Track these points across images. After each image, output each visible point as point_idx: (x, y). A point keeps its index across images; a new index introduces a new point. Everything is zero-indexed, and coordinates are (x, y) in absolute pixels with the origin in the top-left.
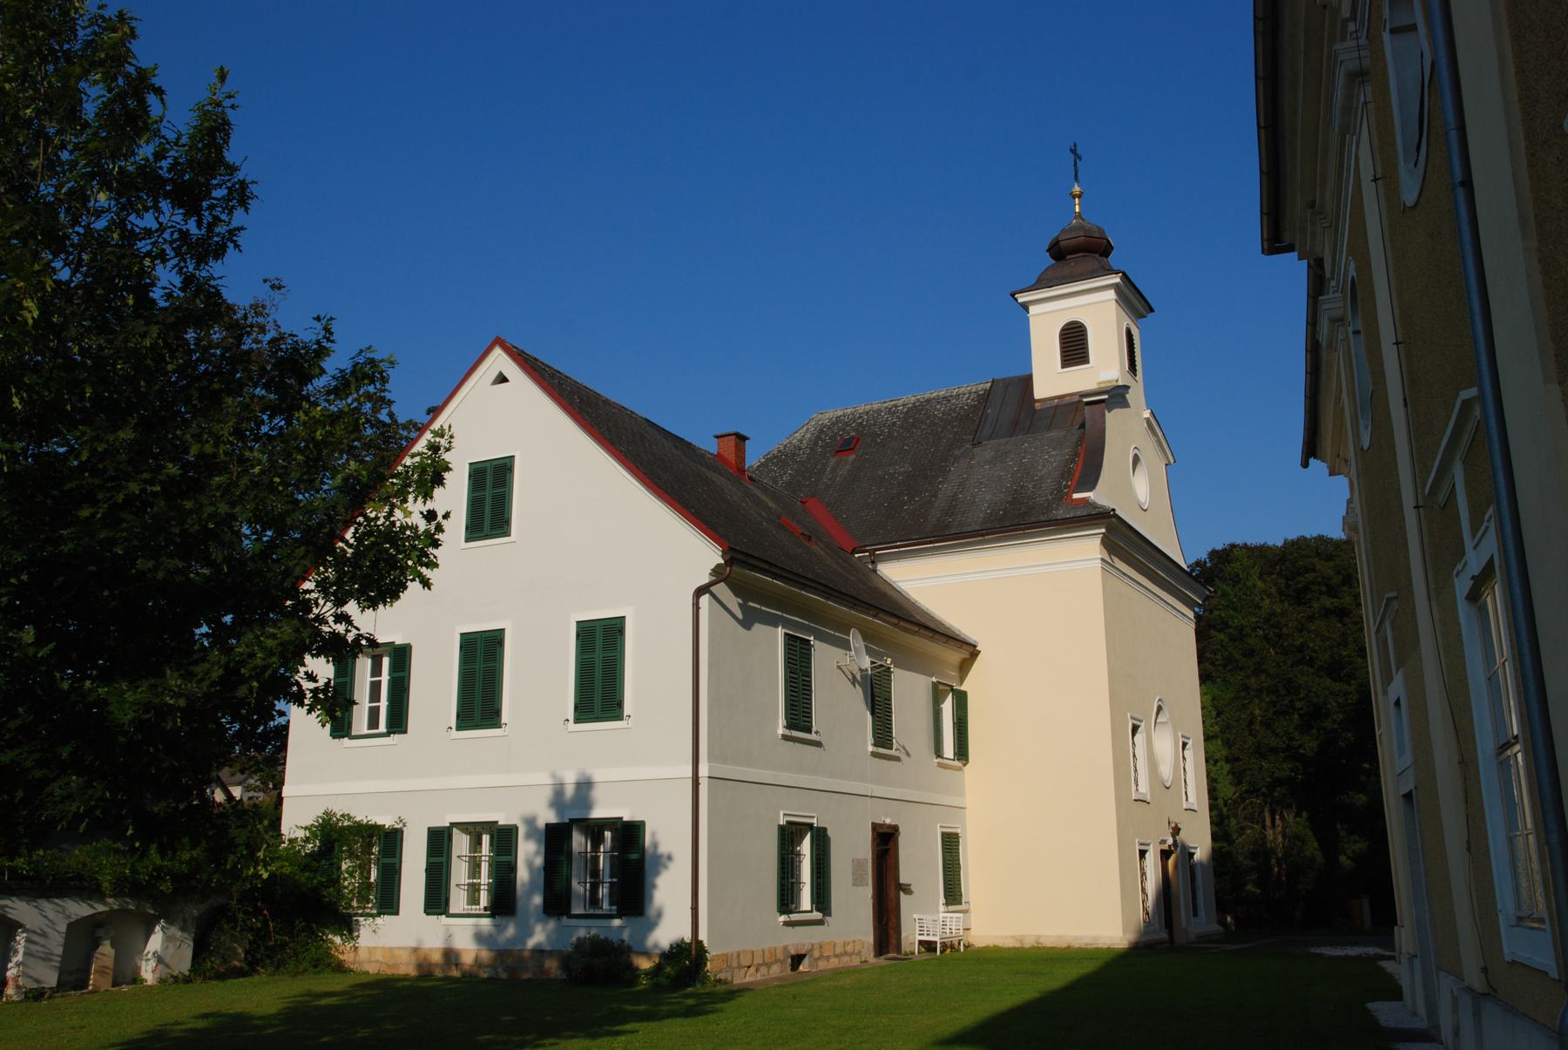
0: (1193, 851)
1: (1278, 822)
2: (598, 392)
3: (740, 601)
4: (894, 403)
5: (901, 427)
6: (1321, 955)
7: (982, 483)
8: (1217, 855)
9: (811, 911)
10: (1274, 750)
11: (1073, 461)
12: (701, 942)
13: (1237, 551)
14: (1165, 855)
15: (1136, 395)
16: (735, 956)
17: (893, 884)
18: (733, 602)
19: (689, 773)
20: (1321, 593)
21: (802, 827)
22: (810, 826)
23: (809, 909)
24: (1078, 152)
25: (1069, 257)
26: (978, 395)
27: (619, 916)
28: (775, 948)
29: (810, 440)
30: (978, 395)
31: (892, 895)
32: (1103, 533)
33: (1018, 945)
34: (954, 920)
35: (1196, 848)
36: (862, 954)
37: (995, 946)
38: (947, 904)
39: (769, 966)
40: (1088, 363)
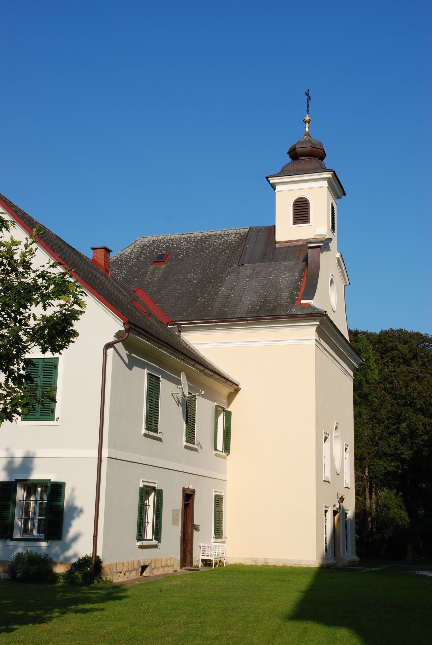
0: (346, 512)
1: (374, 496)
2: (31, 216)
3: (128, 353)
4: (188, 235)
5: (194, 250)
6: (425, 576)
7: (245, 288)
8: (357, 515)
9: (152, 540)
10: (385, 455)
11: (300, 280)
12: (98, 557)
13: (360, 336)
14: (335, 513)
15: (333, 245)
16: (115, 566)
17: (190, 526)
18: (124, 352)
19: (96, 454)
20: (400, 363)
21: (150, 489)
22: (154, 489)
23: (151, 538)
24: (310, 95)
25: (300, 158)
26: (241, 235)
27: (45, 540)
28: (134, 561)
29: (136, 253)
30: (241, 235)
31: (189, 531)
32: (318, 325)
33: (254, 564)
34: (221, 547)
35: (348, 510)
36: (174, 566)
37: (240, 564)
38: (215, 538)
39: (130, 572)
40: (309, 223)
